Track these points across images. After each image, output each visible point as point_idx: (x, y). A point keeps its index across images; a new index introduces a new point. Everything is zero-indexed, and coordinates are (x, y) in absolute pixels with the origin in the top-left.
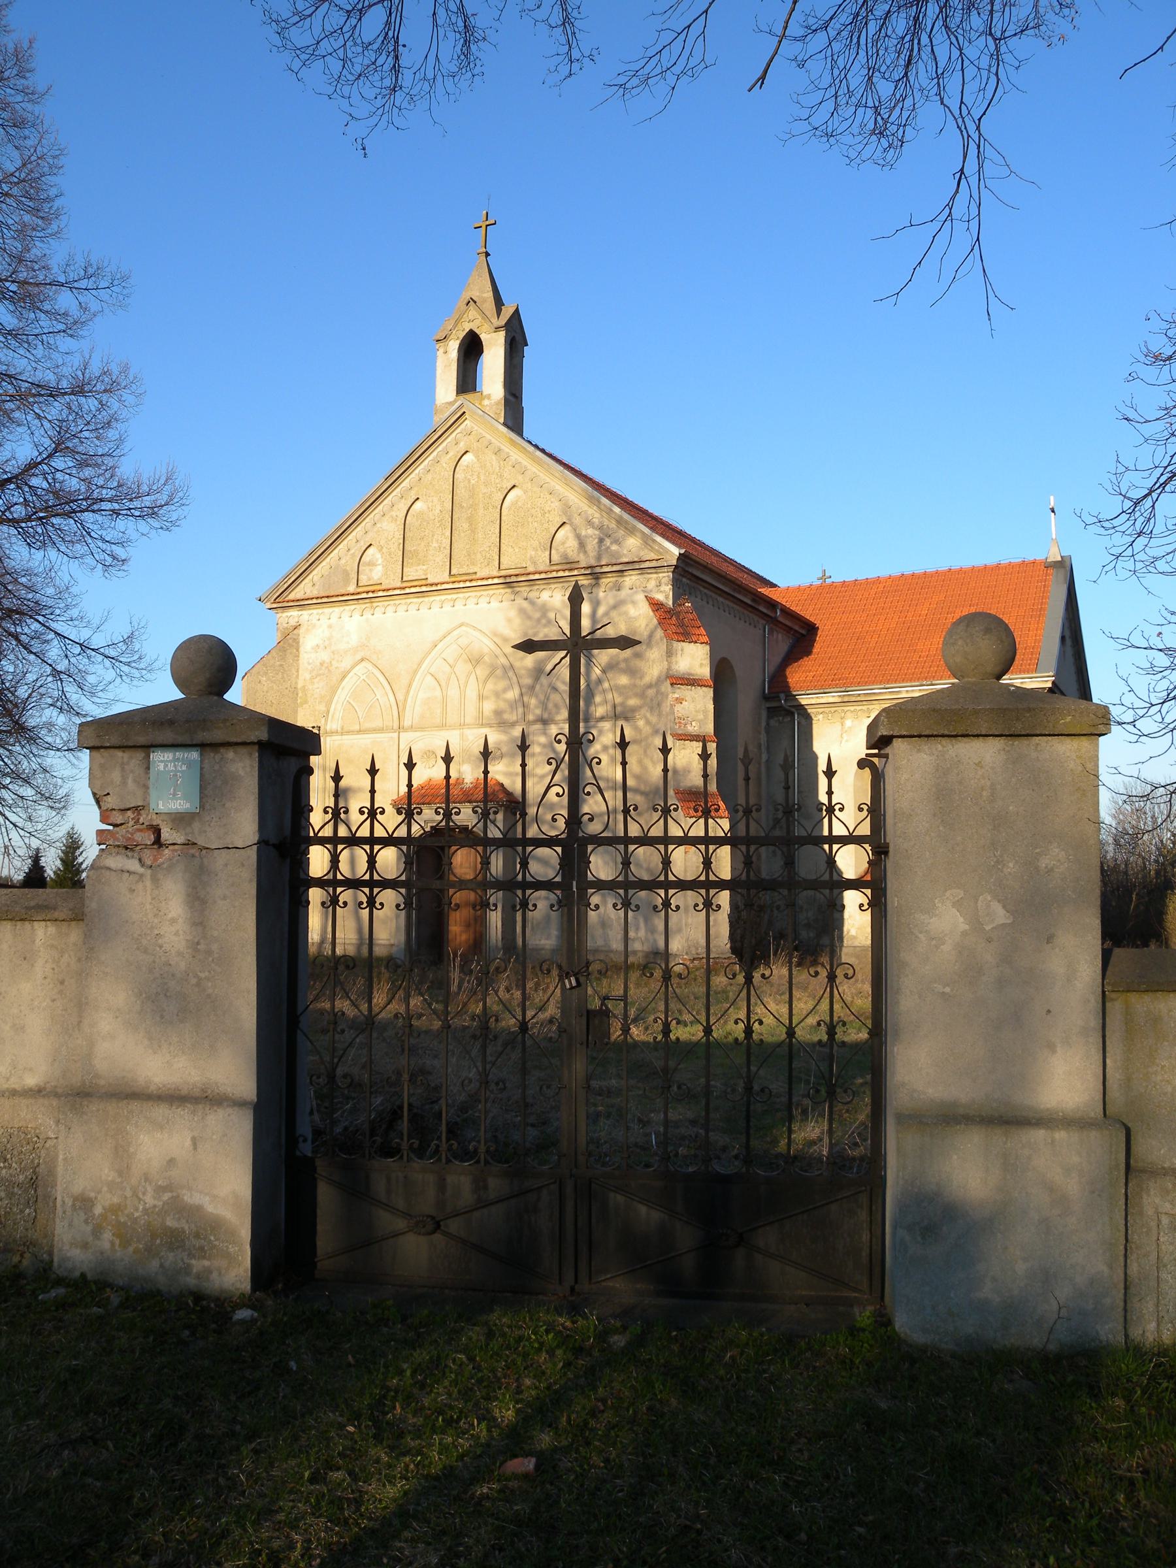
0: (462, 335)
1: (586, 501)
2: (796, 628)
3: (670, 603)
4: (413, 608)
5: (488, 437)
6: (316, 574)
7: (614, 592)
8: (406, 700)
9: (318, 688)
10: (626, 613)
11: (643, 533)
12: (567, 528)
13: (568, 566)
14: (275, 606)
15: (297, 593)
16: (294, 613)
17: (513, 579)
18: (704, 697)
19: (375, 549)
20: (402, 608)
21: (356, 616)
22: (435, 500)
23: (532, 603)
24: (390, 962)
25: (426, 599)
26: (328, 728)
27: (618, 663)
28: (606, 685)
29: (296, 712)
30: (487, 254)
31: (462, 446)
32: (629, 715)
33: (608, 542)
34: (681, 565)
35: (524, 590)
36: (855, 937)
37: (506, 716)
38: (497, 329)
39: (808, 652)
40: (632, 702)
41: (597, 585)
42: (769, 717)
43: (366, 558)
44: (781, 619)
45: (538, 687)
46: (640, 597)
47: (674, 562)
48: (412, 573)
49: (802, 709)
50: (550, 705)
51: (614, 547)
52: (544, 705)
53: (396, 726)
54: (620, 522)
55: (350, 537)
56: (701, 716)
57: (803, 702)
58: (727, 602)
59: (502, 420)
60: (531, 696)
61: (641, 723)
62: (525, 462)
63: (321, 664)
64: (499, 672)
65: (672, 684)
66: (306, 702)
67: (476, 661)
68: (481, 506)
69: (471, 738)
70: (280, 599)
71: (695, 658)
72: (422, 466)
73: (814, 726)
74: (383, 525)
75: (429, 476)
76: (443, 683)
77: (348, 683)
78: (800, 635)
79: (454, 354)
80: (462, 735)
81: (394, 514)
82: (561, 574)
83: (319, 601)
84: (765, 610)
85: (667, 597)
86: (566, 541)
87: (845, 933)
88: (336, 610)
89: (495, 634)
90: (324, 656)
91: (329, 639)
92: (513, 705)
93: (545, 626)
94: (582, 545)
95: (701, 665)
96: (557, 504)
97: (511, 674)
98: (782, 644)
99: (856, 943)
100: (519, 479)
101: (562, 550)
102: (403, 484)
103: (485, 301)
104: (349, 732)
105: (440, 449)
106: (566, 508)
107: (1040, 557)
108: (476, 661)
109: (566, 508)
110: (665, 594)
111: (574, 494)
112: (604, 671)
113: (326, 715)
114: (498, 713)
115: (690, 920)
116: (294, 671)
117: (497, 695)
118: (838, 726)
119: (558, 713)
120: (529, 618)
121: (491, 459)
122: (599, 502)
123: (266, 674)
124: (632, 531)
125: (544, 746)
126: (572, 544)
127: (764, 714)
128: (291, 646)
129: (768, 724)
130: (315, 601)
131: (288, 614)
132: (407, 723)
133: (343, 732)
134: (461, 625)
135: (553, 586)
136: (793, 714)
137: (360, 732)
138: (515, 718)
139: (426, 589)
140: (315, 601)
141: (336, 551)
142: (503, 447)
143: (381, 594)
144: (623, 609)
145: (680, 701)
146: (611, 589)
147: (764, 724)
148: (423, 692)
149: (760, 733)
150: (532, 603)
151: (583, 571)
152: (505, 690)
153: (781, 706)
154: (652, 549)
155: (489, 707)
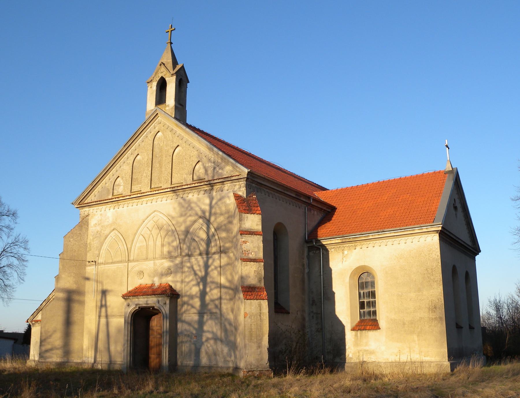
0: (158, 79)
1: (208, 150)
2: (325, 208)
3: (245, 196)
4: (135, 204)
5: (168, 124)
6: (96, 191)
7: (221, 192)
8: (131, 248)
9: (95, 243)
10: (225, 202)
11: (232, 163)
12: (200, 163)
13: (200, 181)
14: (79, 206)
15: (88, 200)
16: (87, 209)
17: (176, 188)
18: (258, 240)
19: (120, 178)
20: (130, 205)
21: (112, 210)
22: (145, 154)
23: (184, 200)
24: (120, 373)
25: (140, 200)
26: (99, 262)
27: (221, 227)
28: (217, 237)
29: (86, 255)
30: (171, 43)
31: (157, 129)
32: (227, 251)
33: (217, 169)
34: (249, 177)
35: (180, 193)
36: (351, 358)
37: (173, 254)
38: (172, 75)
39: (329, 220)
40: (228, 245)
41: (212, 189)
42: (309, 251)
43: (116, 183)
44: (313, 204)
45: (187, 239)
46: (231, 195)
47: (246, 176)
48: (135, 188)
49: (323, 246)
50: (192, 248)
51: (220, 171)
52: (189, 248)
53: (127, 260)
54: (222, 159)
55: (110, 174)
56: (256, 250)
57: (324, 243)
58: (281, 196)
59: (173, 116)
60: (184, 244)
61: (231, 255)
62: (183, 134)
63: (97, 232)
64: (170, 233)
65: (241, 234)
66: (90, 250)
67: (160, 228)
68: (164, 156)
69: (158, 264)
70: (81, 203)
71: (253, 221)
72: (140, 140)
73: (330, 255)
74: (123, 168)
75: (143, 144)
76: (147, 239)
77: (109, 239)
78: (327, 212)
79: (154, 88)
80: (154, 263)
81: (128, 162)
82: (197, 185)
83: (96, 203)
84: (304, 200)
85: (243, 193)
86: (200, 170)
87: (347, 356)
88: (104, 207)
89: (169, 215)
90: (98, 228)
91: (100, 220)
92: (176, 248)
93: (190, 210)
94: (206, 171)
95: (257, 225)
96: (196, 153)
97: (175, 233)
98: (318, 216)
99: (352, 361)
100: (180, 142)
101: (198, 174)
102: (132, 148)
103: (168, 63)
104: (108, 263)
105: (148, 131)
106: (200, 154)
107: (442, 169)
108: (160, 228)
109: (200, 154)
110: (242, 192)
111: (201, 146)
112: (215, 230)
113: (98, 256)
114: (169, 252)
115: (247, 352)
116: (86, 236)
117: (169, 244)
118: (341, 254)
119: (195, 252)
120: (183, 207)
121: (169, 134)
122: (213, 150)
123: (73, 237)
124: (227, 163)
125: (189, 268)
126: (202, 171)
127: (306, 250)
128: (84, 224)
129: (309, 254)
130: (94, 203)
131: (84, 210)
132: (131, 258)
133: (105, 263)
134: (154, 211)
135: (194, 191)
136: (320, 249)
137: (112, 263)
138: (177, 254)
139: (140, 195)
140: (94, 203)
141: (104, 180)
142: (174, 128)
143: (121, 198)
144: (223, 201)
145: (245, 242)
146: (219, 191)
147: (306, 254)
148: (139, 243)
149: (303, 259)
150: (184, 200)
151: (206, 183)
152: (173, 241)
153: (314, 246)
154: (237, 171)
155: (166, 249)
